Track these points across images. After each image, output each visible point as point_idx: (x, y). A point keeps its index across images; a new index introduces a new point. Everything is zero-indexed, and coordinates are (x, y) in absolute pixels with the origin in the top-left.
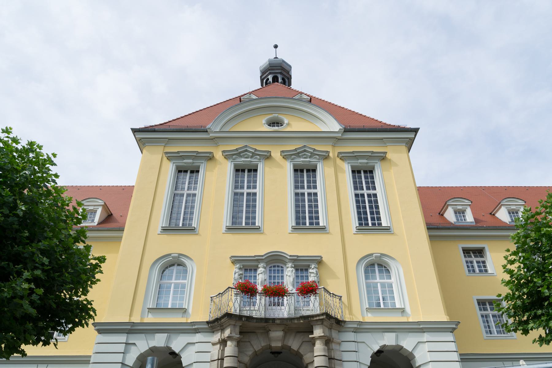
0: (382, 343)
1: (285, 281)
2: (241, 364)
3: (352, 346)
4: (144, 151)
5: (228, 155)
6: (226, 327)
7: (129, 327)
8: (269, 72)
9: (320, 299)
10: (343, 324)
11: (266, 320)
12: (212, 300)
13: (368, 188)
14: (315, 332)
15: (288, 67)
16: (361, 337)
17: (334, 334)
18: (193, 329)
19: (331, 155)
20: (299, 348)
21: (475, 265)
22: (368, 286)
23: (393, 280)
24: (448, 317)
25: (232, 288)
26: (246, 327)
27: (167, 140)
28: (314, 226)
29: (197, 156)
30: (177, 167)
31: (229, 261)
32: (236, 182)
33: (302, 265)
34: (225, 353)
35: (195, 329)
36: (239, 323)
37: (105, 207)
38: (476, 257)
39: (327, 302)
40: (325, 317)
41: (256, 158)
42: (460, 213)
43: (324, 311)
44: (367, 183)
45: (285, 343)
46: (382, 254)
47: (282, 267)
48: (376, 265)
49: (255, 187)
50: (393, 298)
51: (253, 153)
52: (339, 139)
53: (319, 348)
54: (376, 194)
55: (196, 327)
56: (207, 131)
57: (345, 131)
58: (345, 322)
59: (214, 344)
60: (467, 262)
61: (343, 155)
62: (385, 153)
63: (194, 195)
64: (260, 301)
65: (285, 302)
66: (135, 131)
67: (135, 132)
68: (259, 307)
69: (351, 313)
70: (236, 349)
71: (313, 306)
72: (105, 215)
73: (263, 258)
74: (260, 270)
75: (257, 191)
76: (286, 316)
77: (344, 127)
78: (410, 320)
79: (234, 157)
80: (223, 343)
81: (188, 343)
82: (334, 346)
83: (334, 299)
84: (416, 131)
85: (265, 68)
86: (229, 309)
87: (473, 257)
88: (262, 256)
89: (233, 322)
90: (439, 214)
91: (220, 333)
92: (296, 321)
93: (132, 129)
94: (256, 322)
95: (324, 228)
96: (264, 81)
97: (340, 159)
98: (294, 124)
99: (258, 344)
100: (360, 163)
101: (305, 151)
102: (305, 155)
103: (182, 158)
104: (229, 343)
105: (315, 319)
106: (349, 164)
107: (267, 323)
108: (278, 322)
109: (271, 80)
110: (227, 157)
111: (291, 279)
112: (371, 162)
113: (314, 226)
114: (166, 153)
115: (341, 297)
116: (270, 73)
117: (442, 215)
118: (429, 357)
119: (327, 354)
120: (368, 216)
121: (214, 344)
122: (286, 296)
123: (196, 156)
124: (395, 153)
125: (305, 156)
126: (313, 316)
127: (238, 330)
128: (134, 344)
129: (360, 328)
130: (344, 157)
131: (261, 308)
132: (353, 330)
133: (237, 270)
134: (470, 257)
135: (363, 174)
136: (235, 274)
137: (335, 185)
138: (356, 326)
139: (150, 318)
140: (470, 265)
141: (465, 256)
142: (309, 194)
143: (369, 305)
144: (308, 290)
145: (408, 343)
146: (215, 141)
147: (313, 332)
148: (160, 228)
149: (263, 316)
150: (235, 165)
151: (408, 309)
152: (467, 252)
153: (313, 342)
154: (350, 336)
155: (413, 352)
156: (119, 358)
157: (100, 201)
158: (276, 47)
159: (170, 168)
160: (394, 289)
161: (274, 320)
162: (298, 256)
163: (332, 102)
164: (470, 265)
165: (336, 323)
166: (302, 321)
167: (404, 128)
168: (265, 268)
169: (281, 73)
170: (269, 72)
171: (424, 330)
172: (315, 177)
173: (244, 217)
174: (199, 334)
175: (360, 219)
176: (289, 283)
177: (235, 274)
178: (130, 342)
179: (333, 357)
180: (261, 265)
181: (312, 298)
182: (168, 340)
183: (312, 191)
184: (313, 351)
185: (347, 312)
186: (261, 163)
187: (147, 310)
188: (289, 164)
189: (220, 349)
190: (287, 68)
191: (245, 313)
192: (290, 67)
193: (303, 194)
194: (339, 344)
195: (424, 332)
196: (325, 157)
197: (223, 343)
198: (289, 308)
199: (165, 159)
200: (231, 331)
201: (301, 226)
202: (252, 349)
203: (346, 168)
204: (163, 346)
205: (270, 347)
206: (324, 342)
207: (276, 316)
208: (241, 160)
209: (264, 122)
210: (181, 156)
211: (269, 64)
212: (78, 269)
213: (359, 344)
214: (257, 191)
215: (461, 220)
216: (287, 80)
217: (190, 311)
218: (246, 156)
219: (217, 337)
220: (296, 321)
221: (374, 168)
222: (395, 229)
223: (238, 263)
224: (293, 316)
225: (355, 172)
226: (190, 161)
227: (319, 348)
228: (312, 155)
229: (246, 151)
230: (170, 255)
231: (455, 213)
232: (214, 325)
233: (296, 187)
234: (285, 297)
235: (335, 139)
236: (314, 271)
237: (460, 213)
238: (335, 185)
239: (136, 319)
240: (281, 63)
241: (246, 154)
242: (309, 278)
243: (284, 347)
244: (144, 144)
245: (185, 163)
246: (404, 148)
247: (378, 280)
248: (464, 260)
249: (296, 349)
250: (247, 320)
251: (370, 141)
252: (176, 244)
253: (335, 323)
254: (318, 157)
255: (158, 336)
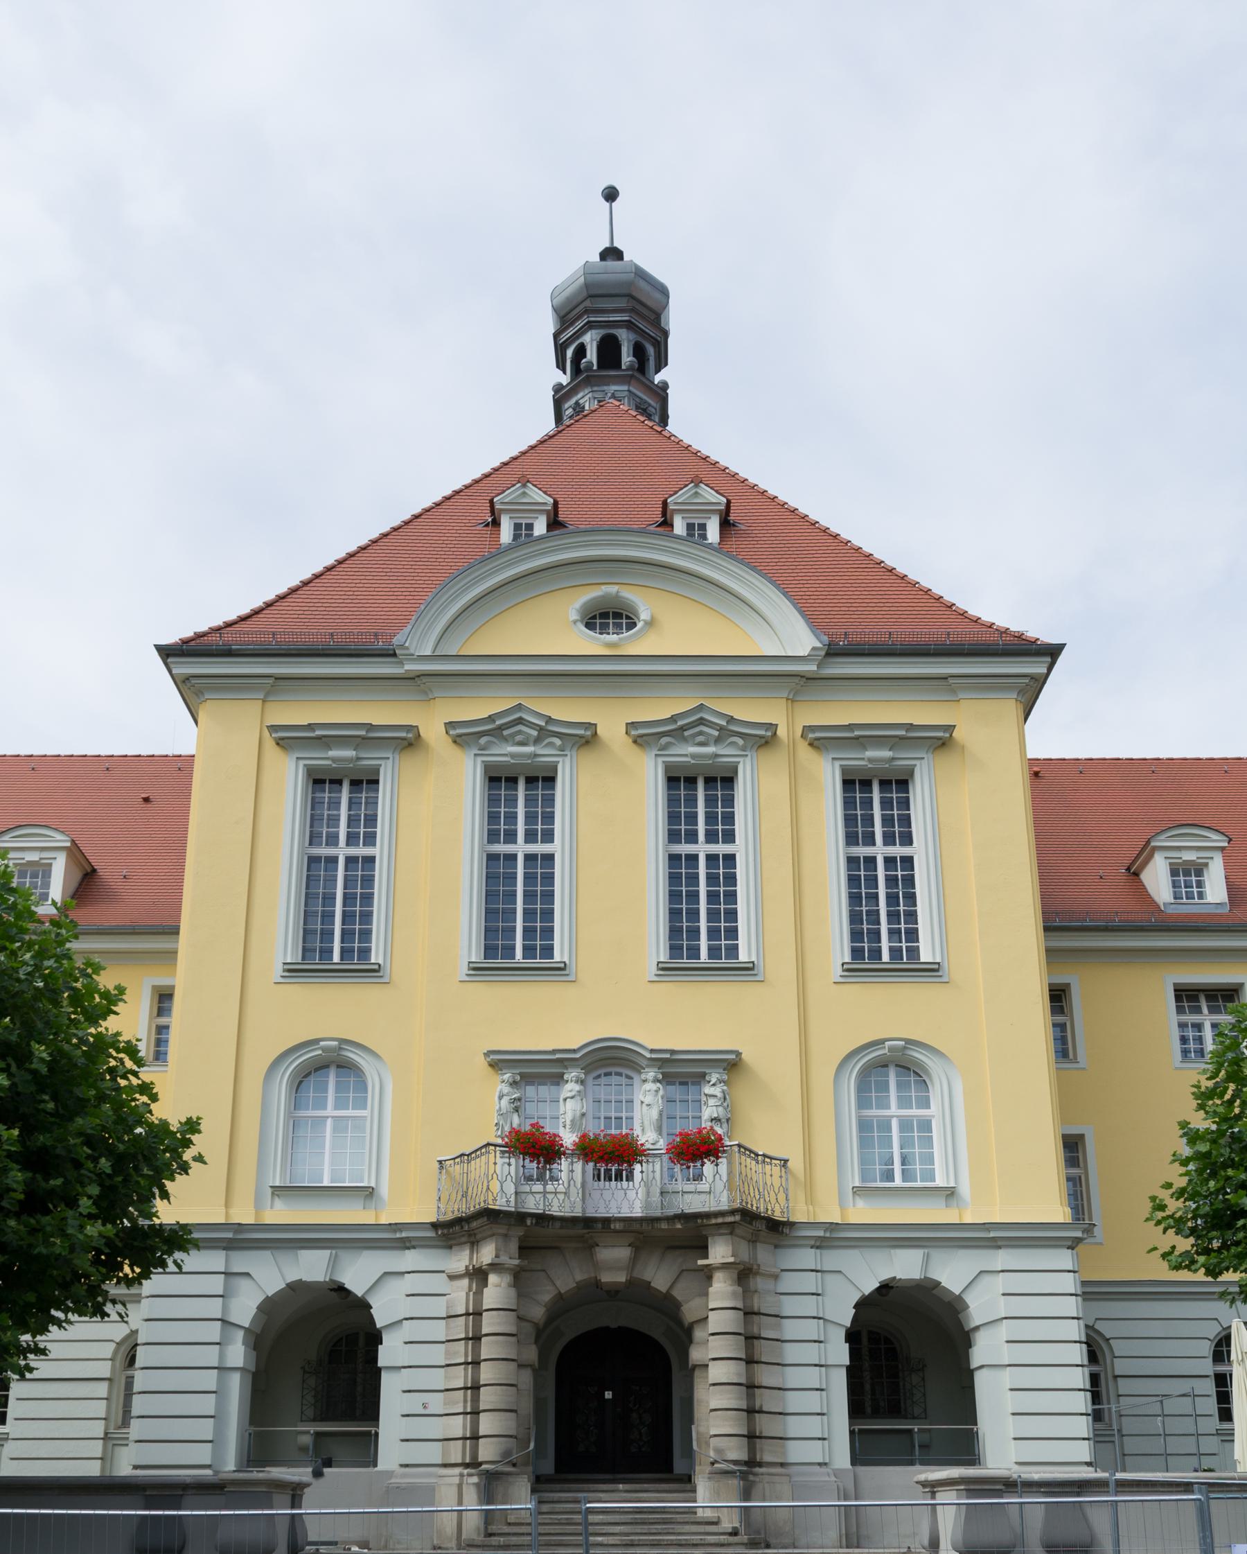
0: (885, 1275)
1: (637, 1115)
2: (524, 1324)
3: (809, 1282)
4: (202, 717)
5: (464, 736)
6: (484, 1238)
7: (230, 1235)
8: (585, 320)
9: (730, 1163)
10: (786, 1230)
11: (587, 1222)
12: (441, 1168)
13: (889, 839)
14: (711, 1251)
15: (658, 296)
16: (832, 1259)
17: (764, 1256)
18: (398, 1238)
19: (782, 732)
20: (671, 1287)
21: (1208, 1033)
22: (864, 1126)
23: (934, 1110)
24: (1068, 1210)
25: (495, 1146)
26: (535, 1238)
27: (271, 681)
28: (723, 962)
29: (368, 737)
30: (310, 771)
31: (482, 1062)
32: (493, 818)
33: (681, 1072)
34: (485, 1301)
35: (401, 1239)
36: (520, 1232)
37: (75, 852)
38: (1213, 1010)
39: (745, 1179)
40: (738, 1218)
41: (551, 744)
42: (1187, 874)
43: (737, 1205)
44: (887, 821)
45: (635, 1275)
46: (908, 1041)
47: (629, 1077)
48: (893, 1067)
49: (548, 837)
50: (930, 1159)
51: (541, 729)
52: (808, 679)
53: (721, 1290)
54: (912, 858)
55: (404, 1235)
56: (394, 655)
57: (828, 654)
58: (791, 1225)
59: (452, 1277)
60: (1182, 1026)
61: (818, 735)
62: (950, 728)
63: (370, 860)
64: (570, 1171)
65: (637, 1175)
66: (167, 653)
67: (168, 656)
68: (567, 1191)
69: (811, 1199)
70: (513, 1292)
71: (710, 1189)
72: (77, 876)
73: (577, 1056)
74: (569, 1086)
75: (554, 847)
76: (638, 1212)
77: (825, 639)
78: (968, 1219)
79: (483, 740)
80: (479, 1275)
81: (386, 1274)
82: (760, 1283)
83: (768, 1167)
84: (1053, 652)
85: (568, 300)
86: (491, 1197)
87: (1205, 1010)
88: (574, 1051)
89: (502, 1230)
90: (1128, 869)
91: (467, 1252)
92: (664, 1226)
93: (159, 648)
94: (561, 1228)
95: (749, 968)
96: (570, 353)
97: (811, 744)
98: (674, 628)
99: (565, 1277)
100: (870, 760)
101: (702, 722)
102: (701, 733)
103: (325, 742)
104: (493, 1278)
105: (714, 1221)
106: (837, 764)
107: (587, 1231)
108: (618, 1226)
109: (592, 355)
110: (459, 741)
111: (654, 1113)
112: (904, 758)
113: (723, 962)
114: (273, 728)
115: (786, 1161)
116: (590, 326)
117: (1136, 874)
118: (1003, 1307)
119: (740, 1305)
120: (882, 924)
121: (452, 1277)
122: (641, 1162)
123: (364, 738)
124: (978, 722)
125: (701, 738)
126: (708, 1215)
127: (514, 1246)
128: (248, 1274)
129: (832, 1237)
130: (819, 739)
131: (573, 1191)
132: (812, 1242)
133: (506, 1089)
134: (1198, 1010)
135: (877, 793)
136: (500, 1098)
137: (789, 827)
138: (821, 1233)
139: (280, 1213)
140: (1190, 1034)
141: (1180, 1010)
142: (712, 859)
143: (863, 1179)
144: (695, 1150)
145: (952, 1272)
146: (420, 684)
147: (706, 1247)
148: (280, 967)
149: (578, 1213)
150: (487, 767)
151: (965, 1190)
152: (1186, 996)
153: (707, 1274)
154: (806, 1257)
155: (964, 1296)
156: (214, 1308)
157: (59, 837)
158: (611, 195)
159: (287, 778)
160: (935, 1134)
161: (606, 1221)
162: (673, 1052)
163: (803, 510)
164: (1190, 1034)
165: (767, 1228)
166: (679, 1226)
167: (1020, 636)
168: (582, 1082)
169: (629, 325)
170: (585, 320)
171: (1000, 1243)
172: (729, 801)
173: (517, 923)
174: (412, 1251)
175: (856, 935)
176: (646, 1123)
177: (500, 1098)
178: (235, 1270)
179: (756, 1309)
180: (572, 1074)
181: (708, 1168)
182: (334, 1263)
183: (721, 848)
184: (706, 1295)
185: (801, 1197)
186: (568, 760)
187: (270, 1190)
188: (652, 764)
189: (470, 1290)
190: (652, 298)
191: (533, 1205)
192: (664, 292)
193: (693, 858)
194: (776, 1277)
195: (999, 1247)
196: (764, 739)
197: (479, 1275)
198: (648, 1193)
199: (269, 743)
200: (497, 1250)
201: (685, 962)
202: (550, 1288)
203: (825, 777)
204: (321, 1279)
205: (597, 1284)
206: (735, 1276)
207: (613, 1212)
208: (505, 752)
209: (574, 616)
210: (319, 738)
211: (587, 285)
212: (158, 1163)
213: (828, 1277)
214: (554, 847)
215: (1190, 896)
216: (651, 350)
217: (384, 1191)
218: (518, 738)
219: (460, 1261)
220: (664, 1226)
221: (911, 772)
222: (953, 969)
223: (509, 1068)
224: (658, 1213)
225: (854, 784)
226: (349, 753)
227: (721, 1290)
228: (724, 734)
229: (520, 721)
230: (316, 1041)
231: (1174, 872)
232: (453, 1231)
233: (673, 837)
234: (637, 1167)
235: (797, 680)
236: (717, 1091)
237: (1187, 874)
238: (789, 827)
239: (244, 1214)
240: (630, 284)
241: (520, 732)
242: (704, 1108)
243: (632, 1283)
244: (199, 693)
245: (334, 760)
246: (1009, 707)
247: (894, 1110)
248: (1173, 1018)
249: (663, 1289)
250: (537, 1223)
251: (918, 649)
252: (330, 1011)
253: (765, 1228)
254: (740, 742)
255: (307, 1256)
